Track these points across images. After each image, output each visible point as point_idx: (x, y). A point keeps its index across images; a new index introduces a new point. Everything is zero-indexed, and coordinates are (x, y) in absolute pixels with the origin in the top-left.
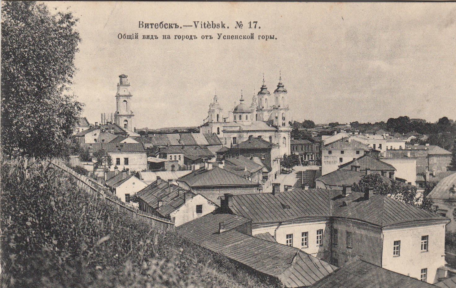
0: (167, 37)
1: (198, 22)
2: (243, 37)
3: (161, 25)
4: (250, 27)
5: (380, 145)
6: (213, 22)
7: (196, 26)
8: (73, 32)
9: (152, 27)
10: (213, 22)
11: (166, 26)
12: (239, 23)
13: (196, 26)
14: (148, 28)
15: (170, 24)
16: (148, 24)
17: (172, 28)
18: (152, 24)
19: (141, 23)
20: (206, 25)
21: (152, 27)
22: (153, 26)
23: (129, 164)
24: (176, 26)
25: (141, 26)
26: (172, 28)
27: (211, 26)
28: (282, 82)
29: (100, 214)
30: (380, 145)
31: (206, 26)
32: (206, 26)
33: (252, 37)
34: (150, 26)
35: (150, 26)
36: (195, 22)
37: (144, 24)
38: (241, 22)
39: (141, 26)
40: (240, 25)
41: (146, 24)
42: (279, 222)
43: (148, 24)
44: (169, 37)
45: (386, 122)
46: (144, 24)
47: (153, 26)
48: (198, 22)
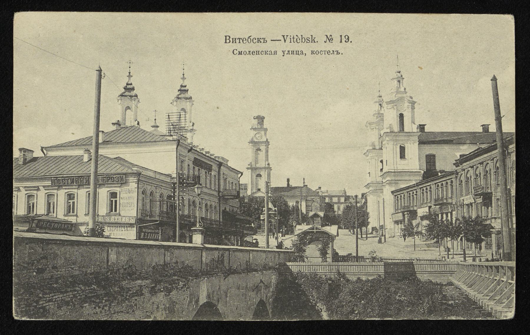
0: (299, 53)
1: (287, 36)
3: (249, 40)
4: (341, 42)
5: (402, 156)
6: (312, 36)
7: (285, 41)
10: (312, 36)
11: (255, 41)
12: (329, 36)
13: (285, 41)
16: (235, 39)
19: (228, 38)
20: (295, 40)
21: (240, 42)
22: (241, 41)
23: (406, 157)
25: (228, 41)
26: (261, 42)
27: (301, 41)
28: (132, 81)
29: (459, 177)
30: (402, 156)
31: (295, 39)
32: (295, 39)
33: (275, 53)
34: (237, 41)
35: (237, 41)
36: (284, 36)
37: (231, 40)
38: (331, 36)
40: (330, 39)
43: (235, 39)
44: (275, 53)
46: (231, 40)
47: (241, 41)
48: (287, 36)
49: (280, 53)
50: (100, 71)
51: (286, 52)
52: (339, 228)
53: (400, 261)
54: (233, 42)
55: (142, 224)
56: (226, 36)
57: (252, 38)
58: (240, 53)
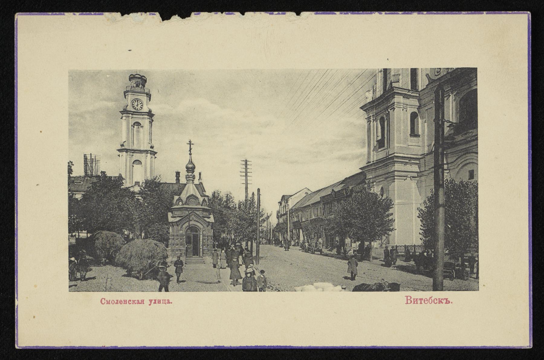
0: (162, 301)
2: (438, 301)
3: (430, 300)
8: (210, 195)
9: (421, 303)
11: (436, 302)
14: (417, 303)
15: (439, 299)
16: (417, 299)
17: (442, 303)
18: (421, 299)
19: (409, 298)
21: (421, 303)
24: (447, 301)
25: (409, 302)
26: (442, 303)
33: (143, 302)
34: (419, 302)
35: (419, 302)
37: (412, 300)
39: (409, 302)
41: (414, 299)
42: (86, 280)
44: (143, 302)
45: (193, 14)
46: (412, 300)
47: (423, 302)
49: (147, 302)
50: (246, 161)
51: (153, 301)
52: (79, 233)
53: (441, 178)
54: (414, 303)
55: (223, 238)
56: (407, 297)
57: (433, 299)
58: (108, 303)
